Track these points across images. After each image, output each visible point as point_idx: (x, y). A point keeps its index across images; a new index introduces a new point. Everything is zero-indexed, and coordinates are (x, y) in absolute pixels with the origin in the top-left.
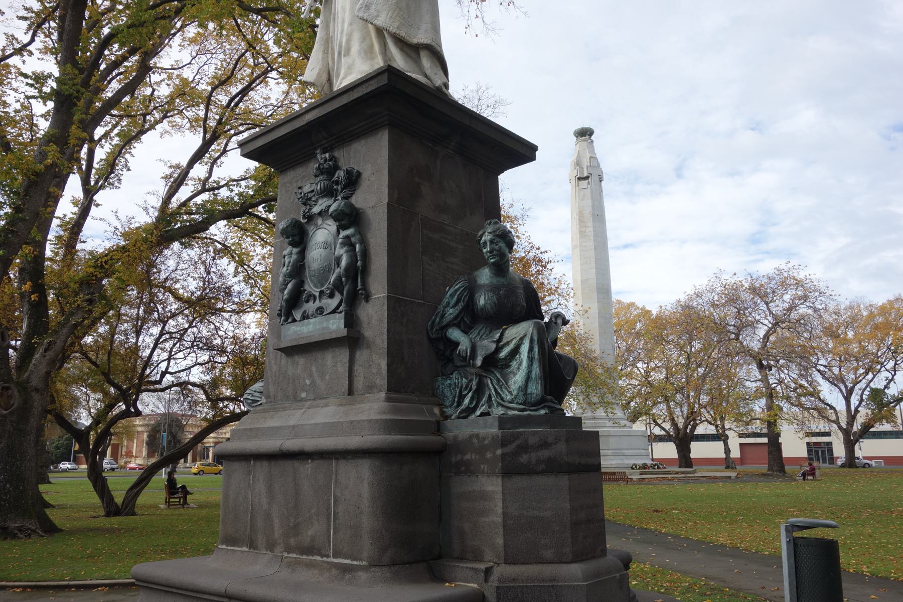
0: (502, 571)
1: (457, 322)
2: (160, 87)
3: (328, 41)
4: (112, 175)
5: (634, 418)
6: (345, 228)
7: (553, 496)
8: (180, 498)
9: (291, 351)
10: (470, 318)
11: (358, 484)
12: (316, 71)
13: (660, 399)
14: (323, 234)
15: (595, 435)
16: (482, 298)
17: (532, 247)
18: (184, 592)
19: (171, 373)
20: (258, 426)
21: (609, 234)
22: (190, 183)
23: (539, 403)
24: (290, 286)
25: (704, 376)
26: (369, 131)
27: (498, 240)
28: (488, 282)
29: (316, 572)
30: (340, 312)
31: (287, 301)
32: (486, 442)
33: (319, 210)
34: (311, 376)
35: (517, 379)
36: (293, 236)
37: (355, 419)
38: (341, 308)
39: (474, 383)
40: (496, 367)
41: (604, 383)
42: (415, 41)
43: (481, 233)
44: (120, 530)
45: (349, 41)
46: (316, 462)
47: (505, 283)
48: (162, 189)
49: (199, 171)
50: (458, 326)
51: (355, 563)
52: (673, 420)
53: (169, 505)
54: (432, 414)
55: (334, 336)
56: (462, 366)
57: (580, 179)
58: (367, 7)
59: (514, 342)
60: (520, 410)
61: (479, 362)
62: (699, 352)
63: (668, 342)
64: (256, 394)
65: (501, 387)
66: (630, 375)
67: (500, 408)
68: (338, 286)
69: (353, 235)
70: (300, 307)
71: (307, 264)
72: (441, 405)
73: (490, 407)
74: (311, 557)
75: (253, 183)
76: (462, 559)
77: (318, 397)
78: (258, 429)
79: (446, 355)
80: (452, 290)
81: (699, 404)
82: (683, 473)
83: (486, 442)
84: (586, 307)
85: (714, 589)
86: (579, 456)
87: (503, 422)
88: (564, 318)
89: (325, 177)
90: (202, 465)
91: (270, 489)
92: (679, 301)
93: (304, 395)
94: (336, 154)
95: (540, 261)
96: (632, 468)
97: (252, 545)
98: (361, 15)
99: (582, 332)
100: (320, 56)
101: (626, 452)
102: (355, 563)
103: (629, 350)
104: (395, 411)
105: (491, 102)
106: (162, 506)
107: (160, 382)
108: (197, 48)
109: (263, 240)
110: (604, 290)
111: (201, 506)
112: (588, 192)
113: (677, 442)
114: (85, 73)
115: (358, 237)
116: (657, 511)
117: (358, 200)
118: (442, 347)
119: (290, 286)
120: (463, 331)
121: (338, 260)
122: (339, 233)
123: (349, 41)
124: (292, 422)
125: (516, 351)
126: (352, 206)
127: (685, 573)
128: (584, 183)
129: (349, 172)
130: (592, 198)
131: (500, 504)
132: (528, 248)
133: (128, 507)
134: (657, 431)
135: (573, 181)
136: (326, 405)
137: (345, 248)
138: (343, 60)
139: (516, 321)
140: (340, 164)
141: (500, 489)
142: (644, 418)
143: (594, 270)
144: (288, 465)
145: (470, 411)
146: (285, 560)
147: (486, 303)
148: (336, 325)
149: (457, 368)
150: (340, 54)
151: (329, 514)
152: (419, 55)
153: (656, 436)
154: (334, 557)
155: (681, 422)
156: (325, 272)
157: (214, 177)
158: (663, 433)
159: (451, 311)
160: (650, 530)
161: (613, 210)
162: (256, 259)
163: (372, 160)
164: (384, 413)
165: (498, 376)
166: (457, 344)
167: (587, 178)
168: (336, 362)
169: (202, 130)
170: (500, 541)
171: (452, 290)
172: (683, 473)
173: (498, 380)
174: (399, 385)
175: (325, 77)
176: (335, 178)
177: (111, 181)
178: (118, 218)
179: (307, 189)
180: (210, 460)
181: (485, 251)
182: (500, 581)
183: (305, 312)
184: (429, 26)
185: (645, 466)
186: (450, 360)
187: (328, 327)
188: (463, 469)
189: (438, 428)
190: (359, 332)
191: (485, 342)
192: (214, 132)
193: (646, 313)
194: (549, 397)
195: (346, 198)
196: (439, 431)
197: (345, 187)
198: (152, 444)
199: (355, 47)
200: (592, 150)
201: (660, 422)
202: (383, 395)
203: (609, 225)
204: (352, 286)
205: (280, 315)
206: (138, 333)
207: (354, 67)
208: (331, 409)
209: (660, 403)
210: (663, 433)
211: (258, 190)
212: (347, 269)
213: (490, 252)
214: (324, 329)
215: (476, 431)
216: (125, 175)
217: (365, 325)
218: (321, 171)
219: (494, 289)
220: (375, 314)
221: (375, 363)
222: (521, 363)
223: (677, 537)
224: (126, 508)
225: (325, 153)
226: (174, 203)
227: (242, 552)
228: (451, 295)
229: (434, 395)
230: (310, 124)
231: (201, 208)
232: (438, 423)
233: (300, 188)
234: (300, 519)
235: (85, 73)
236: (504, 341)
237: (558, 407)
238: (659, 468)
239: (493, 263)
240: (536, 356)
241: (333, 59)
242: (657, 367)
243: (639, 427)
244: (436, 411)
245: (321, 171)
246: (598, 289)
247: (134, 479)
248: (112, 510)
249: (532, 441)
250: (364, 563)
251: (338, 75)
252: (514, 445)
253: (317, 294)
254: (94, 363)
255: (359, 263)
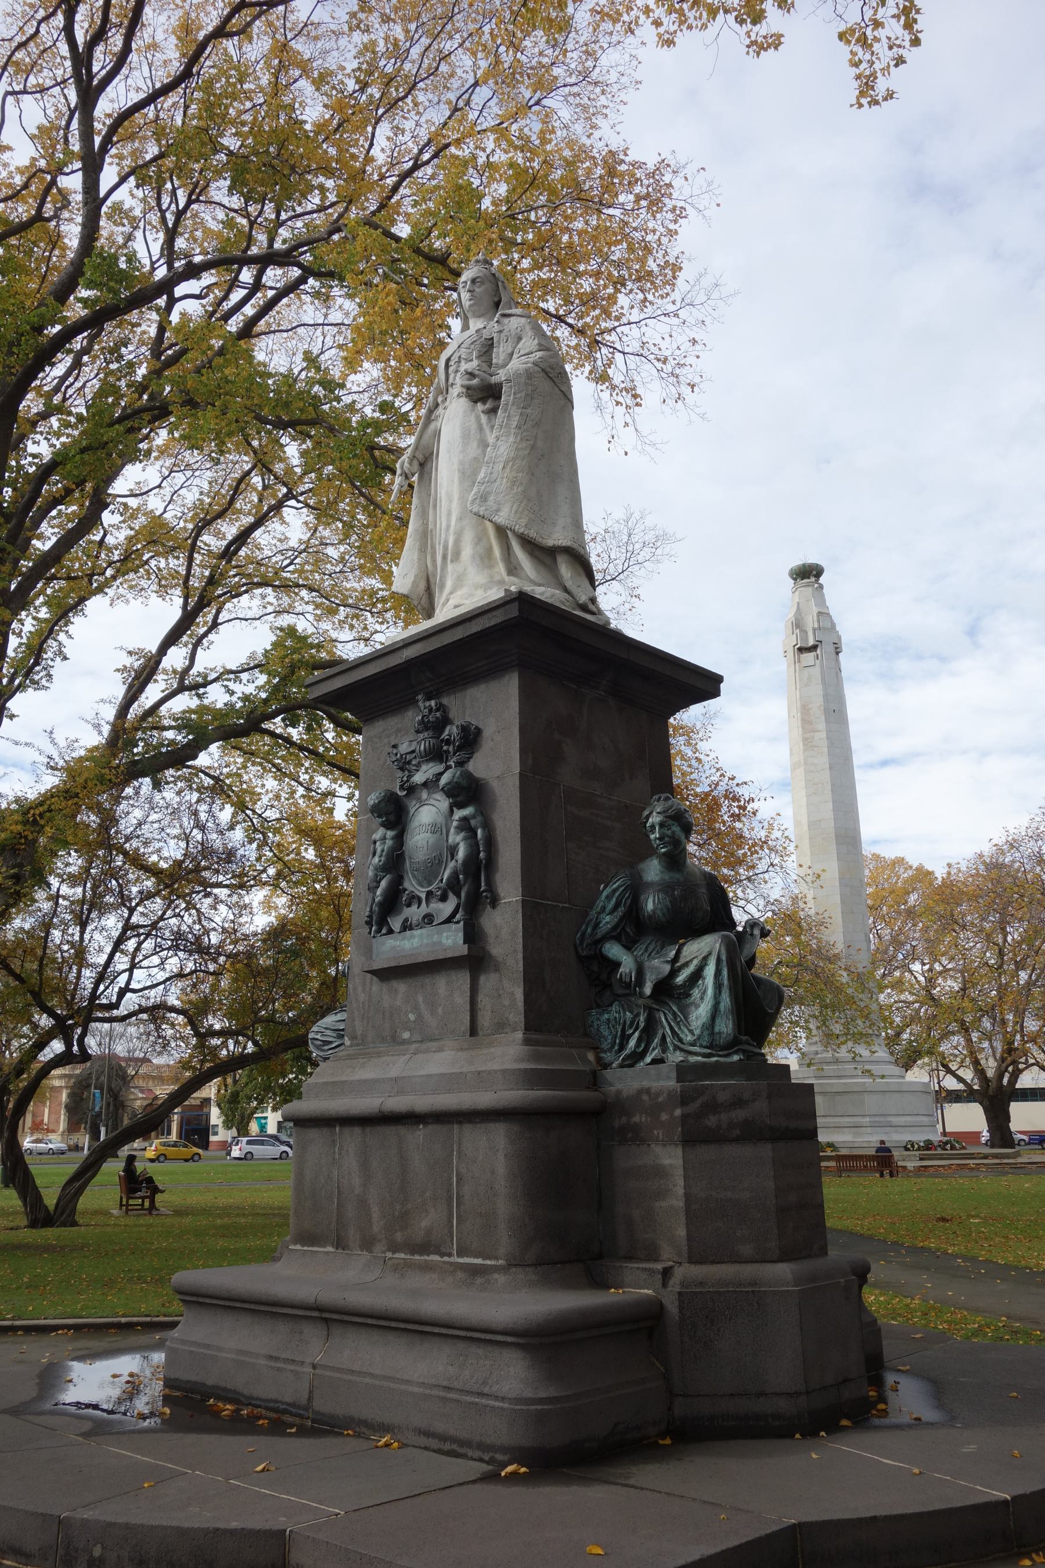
0: (684, 1272)
1: (616, 935)
2: (115, 529)
3: (425, 536)
4: (37, 668)
5: (908, 1064)
6: (461, 806)
7: (751, 1172)
8: (143, 1198)
9: (386, 974)
10: (634, 928)
11: (490, 1159)
12: (411, 578)
13: (954, 1026)
14: (428, 814)
15: (808, 1090)
16: (650, 901)
17: (722, 775)
18: (252, 1307)
19: (134, 991)
20: (344, 1078)
21: (855, 744)
22: (160, 677)
23: (731, 1046)
24: (384, 883)
25: (1030, 984)
26: (491, 672)
27: (671, 822)
28: (657, 879)
29: (435, 1276)
30: (458, 922)
31: (381, 904)
32: (660, 1099)
33: (423, 780)
34: (416, 1008)
35: (700, 1014)
36: (387, 814)
37: (483, 1068)
38: (458, 917)
39: (642, 1018)
40: (671, 996)
41: (851, 1000)
42: (550, 543)
43: (646, 813)
44: (62, 1248)
45: (458, 542)
46: (430, 1127)
47: (682, 879)
48: (119, 691)
49: (176, 657)
50: (618, 939)
51: (488, 1262)
52: (976, 1063)
53: (127, 1211)
54: (586, 1061)
55: (450, 955)
56: (624, 995)
57: (801, 650)
58: (484, 498)
59: (695, 962)
60: (705, 1056)
61: (648, 990)
62: (1020, 943)
63: (964, 927)
64: (328, 1033)
65: (678, 1024)
66: (898, 985)
67: (678, 1053)
68: (454, 885)
69: (474, 817)
70: (399, 913)
71: (407, 853)
72: (596, 1049)
73: (664, 1052)
74: (426, 1257)
75: (262, 679)
76: (630, 1258)
77: (427, 1038)
78: (343, 1083)
79: (601, 979)
80: (608, 890)
81: (1022, 1036)
82: (996, 1156)
83: (660, 1099)
84: (817, 869)
85: (1016, 1333)
86: (788, 1116)
87: (683, 1071)
88: (762, 929)
89: (431, 733)
90: (164, 1144)
91: (365, 1165)
92: (981, 856)
93: (406, 1035)
94: (445, 701)
95: (736, 799)
96: (906, 1149)
97: (340, 1243)
98: (475, 510)
99: (812, 912)
100: (416, 557)
101: (895, 1120)
102: (488, 1262)
103: (897, 942)
104: (536, 1057)
105: (650, 537)
106: (115, 1212)
107: (116, 1006)
108: (169, 462)
109: (279, 770)
110: (847, 836)
111: (179, 1213)
112: (816, 672)
113: (986, 1102)
114: (14, 521)
115: (479, 818)
116: (944, 1220)
117: (478, 766)
118: (595, 968)
119: (384, 883)
120: (625, 947)
121: (453, 851)
122: (452, 812)
123: (458, 542)
124: (394, 1072)
125: (697, 975)
126: (468, 776)
127: (977, 1311)
128: (808, 658)
129: (465, 729)
130: (824, 682)
131: (681, 1182)
132: (715, 778)
133: (65, 1213)
134: (950, 1083)
135: (790, 654)
136: (440, 1050)
137: (462, 834)
138: (450, 567)
139: (697, 932)
140: (451, 716)
141: (681, 1162)
142: (926, 1060)
143: (830, 806)
144: (390, 1132)
145: (637, 1057)
146: (390, 1263)
147: (655, 909)
148: (451, 940)
149: (616, 997)
150: (445, 557)
151: (451, 1198)
152: (555, 560)
153: (950, 1093)
154: (459, 1256)
155: (991, 1067)
156: (434, 866)
157: (198, 667)
158: (961, 1086)
159: (608, 918)
160: (929, 1250)
161: (861, 704)
162: (265, 800)
163: (496, 710)
164: (523, 1060)
165: (675, 1008)
166: (618, 964)
167: (814, 648)
168: (452, 989)
169: (178, 591)
170: (682, 1232)
171: (608, 890)
172: (996, 1156)
173: (675, 1014)
174: (540, 1022)
175: (422, 585)
176: (445, 735)
177: (36, 678)
178: (53, 742)
179: (404, 748)
180: (174, 1137)
181: (652, 837)
182: (682, 1284)
183: (406, 920)
184: (569, 520)
185: (929, 1145)
186: (607, 985)
187: (440, 943)
188: (630, 1135)
189: (594, 1080)
190: (483, 948)
191: (656, 962)
192: (202, 597)
193: (923, 875)
194: (744, 1038)
195: (460, 764)
196: (595, 1084)
197: (459, 749)
198: (78, 1112)
199: (467, 551)
200: (821, 600)
201: (953, 1066)
202: (519, 1035)
203: (853, 729)
204: (473, 885)
205: (369, 923)
206: (83, 926)
207: (468, 590)
208: (448, 1055)
209: (953, 1033)
210: (961, 1086)
211: (275, 691)
212: (466, 862)
213: (660, 839)
214: (434, 944)
215: (646, 1084)
216: (59, 668)
217: (491, 940)
218: (424, 726)
219: (666, 888)
220: (505, 924)
221: (506, 992)
222: (705, 991)
223: (973, 1259)
224: (62, 1214)
225: (429, 699)
226: (135, 711)
227: (327, 1253)
228: (607, 897)
229: (586, 1035)
230: (409, 663)
231: (183, 723)
232: (594, 1073)
233: (395, 746)
234: (409, 1206)
235: (14, 521)
236: (682, 961)
237: (757, 1050)
238: (953, 1148)
239: (664, 854)
240: (726, 982)
241: (434, 561)
242: (946, 970)
243: (918, 1075)
244: (591, 1056)
245: (424, 726)
246: (838, 836)
247: (72, 1169)
248: (39, 1217)
249: (722, 1097)
250: (501, 1262)
251: (442, 586)
252: (698, 1103)
253: (423, 896)
254: (17, 977)
255: (482, 855)
